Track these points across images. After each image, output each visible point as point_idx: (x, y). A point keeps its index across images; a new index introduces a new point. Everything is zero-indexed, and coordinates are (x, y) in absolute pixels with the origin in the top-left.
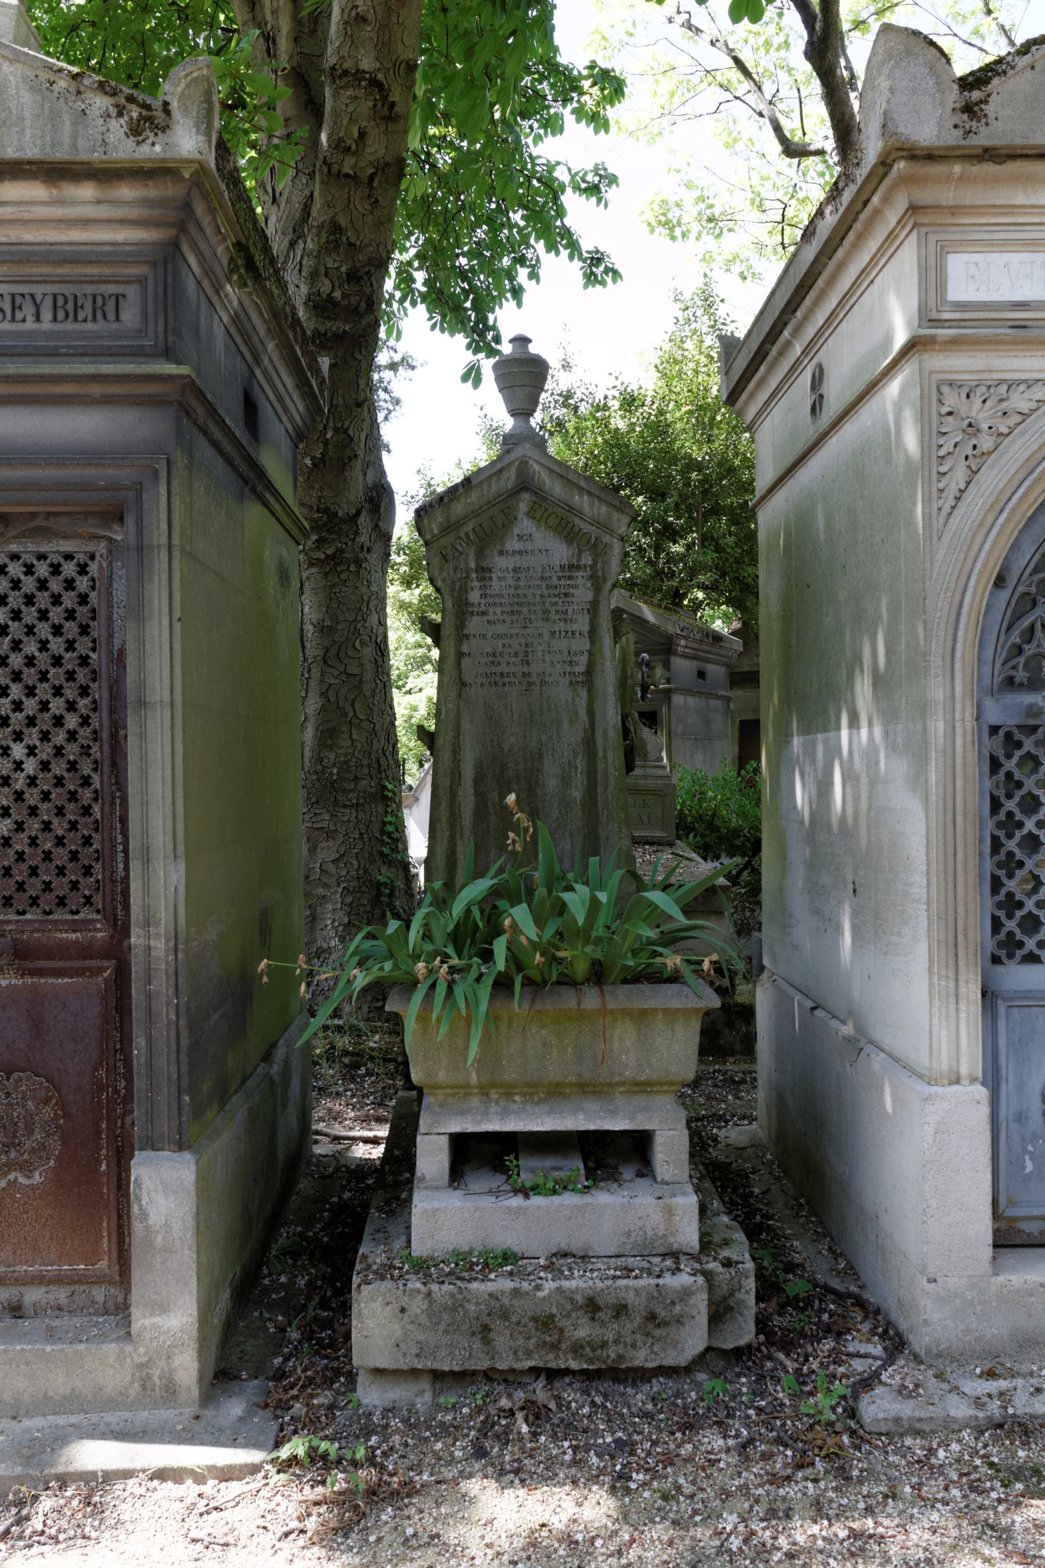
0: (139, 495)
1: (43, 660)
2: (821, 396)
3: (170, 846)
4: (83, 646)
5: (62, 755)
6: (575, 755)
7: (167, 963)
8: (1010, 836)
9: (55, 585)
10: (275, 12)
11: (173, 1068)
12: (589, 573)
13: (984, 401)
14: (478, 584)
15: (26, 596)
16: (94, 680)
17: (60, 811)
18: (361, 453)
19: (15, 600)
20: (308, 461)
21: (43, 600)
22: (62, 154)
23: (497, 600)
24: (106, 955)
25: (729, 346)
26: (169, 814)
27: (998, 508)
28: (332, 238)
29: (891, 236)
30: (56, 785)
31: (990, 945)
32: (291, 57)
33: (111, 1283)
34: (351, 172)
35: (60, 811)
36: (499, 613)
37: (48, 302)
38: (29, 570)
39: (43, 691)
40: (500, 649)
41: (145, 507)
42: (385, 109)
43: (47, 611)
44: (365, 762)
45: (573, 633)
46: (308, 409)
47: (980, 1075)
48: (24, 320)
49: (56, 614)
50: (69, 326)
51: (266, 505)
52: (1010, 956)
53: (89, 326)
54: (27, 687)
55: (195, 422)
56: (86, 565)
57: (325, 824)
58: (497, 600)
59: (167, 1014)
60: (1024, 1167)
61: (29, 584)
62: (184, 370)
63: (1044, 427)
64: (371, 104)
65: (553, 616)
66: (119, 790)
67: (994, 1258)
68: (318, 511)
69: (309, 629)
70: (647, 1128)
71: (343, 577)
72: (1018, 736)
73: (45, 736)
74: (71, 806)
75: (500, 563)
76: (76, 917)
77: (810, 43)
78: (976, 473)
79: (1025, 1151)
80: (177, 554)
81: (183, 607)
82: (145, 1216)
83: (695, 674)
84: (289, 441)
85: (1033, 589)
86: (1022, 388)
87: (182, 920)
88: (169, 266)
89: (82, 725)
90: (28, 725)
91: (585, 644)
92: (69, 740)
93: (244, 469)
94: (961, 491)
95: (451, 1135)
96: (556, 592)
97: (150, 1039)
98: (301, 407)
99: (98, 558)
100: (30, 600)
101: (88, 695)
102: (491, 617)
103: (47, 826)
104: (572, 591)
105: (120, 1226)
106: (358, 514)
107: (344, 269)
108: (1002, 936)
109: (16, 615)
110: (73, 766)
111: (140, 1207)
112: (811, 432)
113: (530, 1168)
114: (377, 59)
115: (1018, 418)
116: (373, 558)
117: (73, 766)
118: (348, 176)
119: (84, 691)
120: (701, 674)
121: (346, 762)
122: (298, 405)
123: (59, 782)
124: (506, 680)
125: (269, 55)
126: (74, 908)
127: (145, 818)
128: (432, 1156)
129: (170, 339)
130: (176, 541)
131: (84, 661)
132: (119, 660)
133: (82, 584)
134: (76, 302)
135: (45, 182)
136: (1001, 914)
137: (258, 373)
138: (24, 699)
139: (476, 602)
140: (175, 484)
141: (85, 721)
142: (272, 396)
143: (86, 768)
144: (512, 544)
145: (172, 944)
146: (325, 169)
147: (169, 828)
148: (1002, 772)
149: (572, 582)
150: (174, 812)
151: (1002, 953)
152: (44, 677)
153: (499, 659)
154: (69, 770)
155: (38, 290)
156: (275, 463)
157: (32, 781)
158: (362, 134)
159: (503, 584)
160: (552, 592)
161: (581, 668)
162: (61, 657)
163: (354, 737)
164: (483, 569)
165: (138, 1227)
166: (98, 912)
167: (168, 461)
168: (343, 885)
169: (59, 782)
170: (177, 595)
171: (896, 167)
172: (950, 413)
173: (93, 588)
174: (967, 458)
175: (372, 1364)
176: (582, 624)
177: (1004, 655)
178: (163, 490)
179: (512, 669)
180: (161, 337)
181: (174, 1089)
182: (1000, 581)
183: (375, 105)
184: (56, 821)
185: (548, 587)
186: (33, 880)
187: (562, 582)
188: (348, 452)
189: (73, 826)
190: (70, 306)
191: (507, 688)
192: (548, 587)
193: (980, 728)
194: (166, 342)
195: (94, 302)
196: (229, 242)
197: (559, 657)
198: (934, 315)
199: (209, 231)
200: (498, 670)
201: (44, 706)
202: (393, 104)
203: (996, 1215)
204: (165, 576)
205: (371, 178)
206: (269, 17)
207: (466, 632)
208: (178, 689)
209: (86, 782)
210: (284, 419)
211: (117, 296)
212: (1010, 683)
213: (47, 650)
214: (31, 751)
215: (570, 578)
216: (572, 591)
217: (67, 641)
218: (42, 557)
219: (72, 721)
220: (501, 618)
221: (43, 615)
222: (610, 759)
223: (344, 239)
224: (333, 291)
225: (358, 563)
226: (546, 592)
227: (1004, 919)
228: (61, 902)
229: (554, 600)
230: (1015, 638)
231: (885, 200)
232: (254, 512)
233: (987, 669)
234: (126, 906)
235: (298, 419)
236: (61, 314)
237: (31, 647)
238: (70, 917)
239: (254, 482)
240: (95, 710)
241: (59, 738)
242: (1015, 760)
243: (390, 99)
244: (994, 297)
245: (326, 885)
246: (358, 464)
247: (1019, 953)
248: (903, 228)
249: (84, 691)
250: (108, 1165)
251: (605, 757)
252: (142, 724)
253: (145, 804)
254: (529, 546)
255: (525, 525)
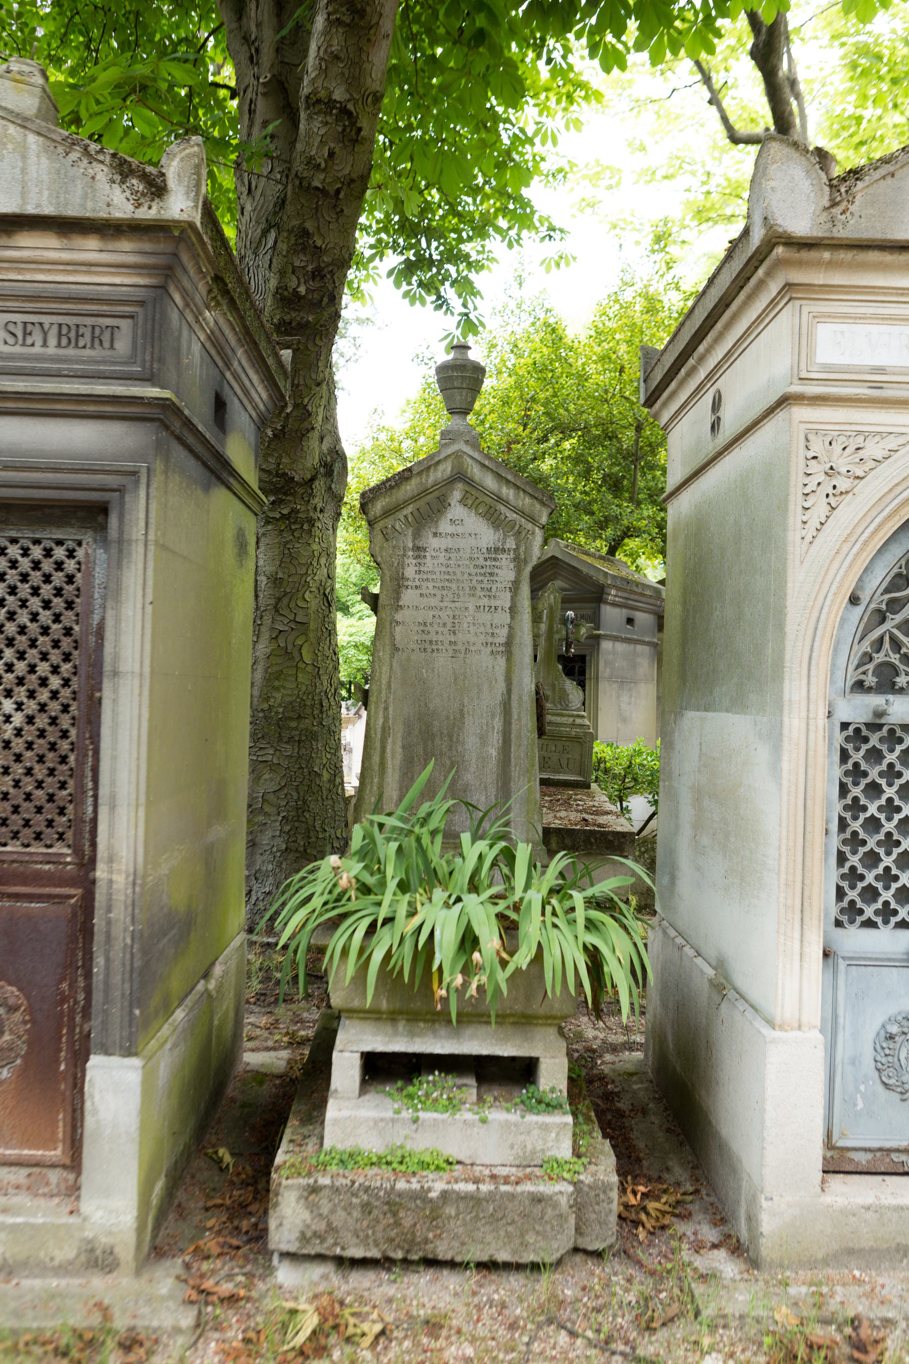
0: (122, 497)
1: (33, 628)
2: (719, 418)
3: (133, 796)
4: (68, 617)
5: (45, 711)
6: (493, 716)
7: (126, 895)
8: (855, 818)
9: (47, 566)
10: (258, 25)
11: (127, 986)
12: (512, 556)
13: (844, 449)
14: (414, 561)
15: (21, 574)
16: (76, 648)
17: (41, 759)
18: (317, 426)
19: (12, 577)
20: (270, 433)
21: (36, 577)
22: (72, 211)
23: (430, 576)
24: (71, 882)
25: (649, 357)
26: (134, 769)
27: (853, 539)
28: (301, 241)
29: (773, 303)
30: (39, 737)
31: (834, 910)
32: (272, 65)
33: (64, 1167)
34: (320, 186)
35: (41, 759)
36: (431, 587)
37: (54, 331)
38: (26, 552)
39: (32, 655)
40: (430, 620)
41: (127, 506)
42: (353, 133)
43: (38, 588)
44: (309, 703)
45: (496, 608)
46: (270, 396)
47: (819, 1024)
48: (33, 345)
49: (46, 591)
50: (71, 352)
51: (229, 488)
52: (852, 922)
53: (87, 352)
54: (18, 652)
55: (172, 433)
56: (74, 550)
57: (269, 758)
58: (430, 576)
59: (124, 939)
60: (855, 1105)
61: (25, 564)
62: (167, 394)
63: (908, 462)
64: (340, 129)
65: (479, 593)
66: (92, 743)
67: (823, 1181)
68: (277, 475)
69: (263, 579)
70: (533, 1055)
71: (296, 534)
72: (865, 732)
73: (31, 695)
74: (51, 755)
75: (433, 543)
76: (50, 851)
77: (755, 46)
78: (834, 509)
79: (858, 1090)
80: (151, 548)
81: (154, 591)
82: (95, 1112)
83: (625, 620)
84: (252, 425)
85: (884, 607)
86: (877, 438)
87: (140, 859)
88: (158, 306)
89: (63, 686)
90: (18, 684)
91: (506, 618)
92: (52, 698)
93: (212, 463)
94: (822, 524)
95: (362, 1053)
96: (482, 571)
97: (108, 960)
98: (264, 396)
99: (84, 546)
100: (24, 578)
101: (70, 661)
102: (424, 591)
103: (29, 772)
104: (496, 571)
105: (74, 1119)
106: (313, 479)
107: (310, 268)
108: (845, 904)
109: (13, 590)
110: (54, 721)
111: (93, 1104)
112: (711, 448)
113: (429, 1084)
114: (347, 91)
115: (873, 464)
116: (326, 518)
117: (54, 721)
118: (317, 188)
119: (67, 657)
120: (630, 621)
121: (291, 702)
122: (261, 393)
123: (42, 734)
124: (434, 647)
125: (252, 62)
126: (48, 842)
127: (114, 771)
128: (345, 1068)
129: (155, 366)
130: (151, 537)
131: (68, 632)
132: (100, 633)
133: (70, 566)
134: (77, 332)
135: (57, 233)
136: (845, 884)
137: (228, 375)
138: (15, 661)
139: (411, 577)
140: (154, 485)
141: (66, 683)
142: (239, 391)
143: (65, 722)
144: (445, 526)
145: (131, 879)
146: (297, 183)
147: (134, 780)
148: (850, 763)
149: (498, 564)
150: (138, 767)
151: (844, 918)
152: (33, 644)
153: (429, 628)
154: (50, 724)
155: (46, 320)
156: (240, 452)
157: (19, 732)
158: (331, 154)
159: (436, 562)
160: (479, 571)
161: (502, 640)
162: (48, 628)
163: (300, 680)
164: (418, 548)
165: (90, 1122)
166: (69, 846)
167: (149, 469)
168: (282, 814)
169: (42, 734)
170: (150, 583)
171: (775, 252)
172: (815, 458)
173: (79, 570)
174: (827, 496)
175: (284, 1247)
176: (505, 600)
177: (856, 662)
178: (142, 493)
179: (440, 638)
180: (148, 365)
181: (126, 1004)
182: (854, 600)
183: (344, 130)
184: (37, 767)
185: (476, 566)
186: (14, 817)
187: (488, 563)
188: (306, 425)
189: (51, 772)
190: (73, 335)
191: (435, 654)
192: (476, 566)
193: (831, 725)
194: (152, 368)
195: (93, 333)
196: (209, 279)
197: (482, 629)
198: (804, 375)
199: (192, 272)
200: (427, 638)
201: (32, 669)
202: (360, 130)
203: (829, 1144)
204: (140, 566)
205: (338, 192)
206: (253, 28)
207: (401, 603)
208: (147, 662)
209: (65, 734)
210: (249, 408)
211: (112, 327)
212: (859, 686)
213: (37, 621)
214: (19, 706)
215: (495, 559)
216: (496, 571)
217: (55, 615)
218: (37, 542)
219: (55, 682)
220: (432, 592)
221: (35, 591)
222: (524, 721)
223: (311, 242)
224: (298, 286)
225: (311, 522)
226: (473, 571)
227: (847, 889)
228: (38, 836)
229: (480, 578)
230: (866, 646)
231: (768, 274)
232: (221, 497)
233: (840, 674)
234: (94, 845)
235: (261, 406)
236: (64, 341)
237: (23, 618)
238: (45, 850)
239: (218, 470)
240: (75, 674)
241: (44, 695)
242: (862, 752)
243: (358, 125)
244: (857, 362)
245: (267, 814)
246: (315, 435)
247: (859, 919)
248: (782, 298)
249: (67, 657)
250: (67, 1065)
251: (519, 719)
252: (115, 691)
253: (114, 758)
254: (460, 529)
255: (456, 511)
